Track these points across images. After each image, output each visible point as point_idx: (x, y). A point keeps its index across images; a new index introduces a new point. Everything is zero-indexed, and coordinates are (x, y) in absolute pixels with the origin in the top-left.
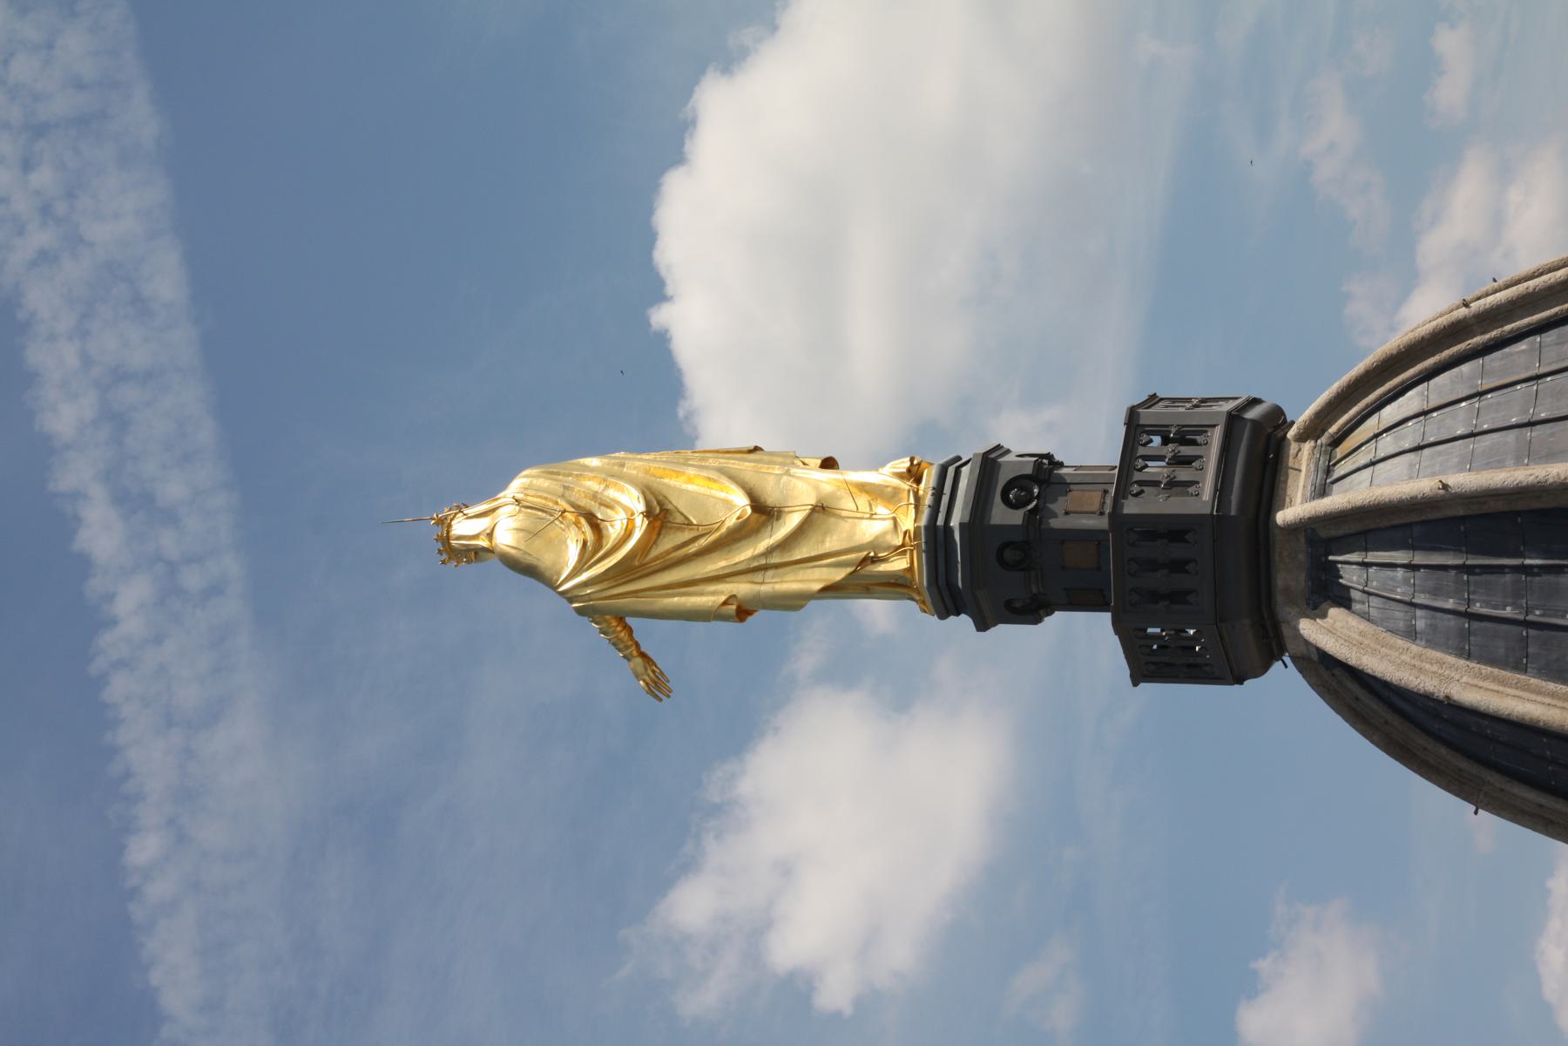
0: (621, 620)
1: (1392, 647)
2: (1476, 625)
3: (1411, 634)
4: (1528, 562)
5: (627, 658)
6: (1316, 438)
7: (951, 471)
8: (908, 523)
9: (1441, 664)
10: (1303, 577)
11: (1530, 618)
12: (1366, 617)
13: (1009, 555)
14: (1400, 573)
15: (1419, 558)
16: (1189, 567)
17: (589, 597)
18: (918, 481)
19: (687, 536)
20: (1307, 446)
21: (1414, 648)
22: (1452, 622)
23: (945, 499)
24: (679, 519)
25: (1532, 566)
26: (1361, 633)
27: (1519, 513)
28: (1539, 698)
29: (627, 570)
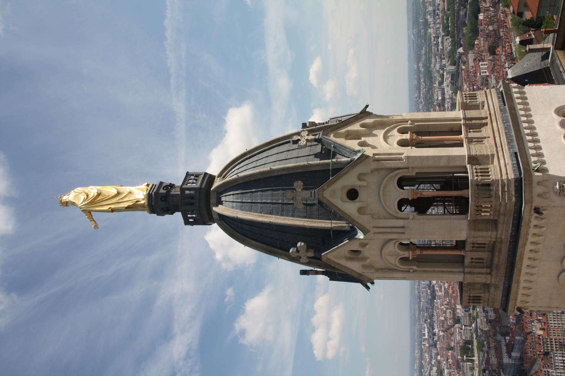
0: (90, 213)
1: (229, 210)
2: (243, 204)
3: (233, 207)
4: (252, 190)
5: (91, 221)
6: (220, 177)
9: (237, 212)
10: (215, 200)
11: (253, 201)
12: (226, 206)
13: (163, 199)
14: (231, 196)
15: (235, 192)
16: (194, 198)
17: (83, 208)
20: (219, 178)
21: (233, 210)
22: (239, 204)
23: (152, 189)
25: (253, 191)
26: (224, 209)
27: (251, 181)
28: (253, 216)
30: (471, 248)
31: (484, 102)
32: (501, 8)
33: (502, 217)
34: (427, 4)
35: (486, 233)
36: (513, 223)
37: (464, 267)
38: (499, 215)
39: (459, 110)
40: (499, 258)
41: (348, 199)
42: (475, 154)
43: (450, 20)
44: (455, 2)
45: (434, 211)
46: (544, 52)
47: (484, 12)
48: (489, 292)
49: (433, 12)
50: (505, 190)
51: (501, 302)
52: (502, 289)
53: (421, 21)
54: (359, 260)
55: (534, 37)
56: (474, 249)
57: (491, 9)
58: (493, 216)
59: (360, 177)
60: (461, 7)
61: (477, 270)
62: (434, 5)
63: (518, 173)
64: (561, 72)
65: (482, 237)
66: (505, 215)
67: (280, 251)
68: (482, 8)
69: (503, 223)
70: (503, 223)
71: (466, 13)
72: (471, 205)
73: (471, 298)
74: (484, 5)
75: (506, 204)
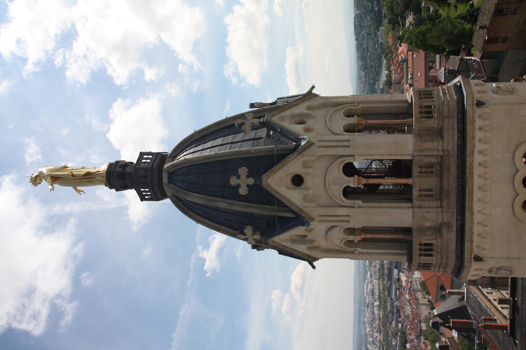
13: (120, 177)
30: (419, 174)
32: (423, 340)
33: (446, 121)
34: (368, 337)
36: (458, 127)
38: (443, 118)
41: (293, 185)
43: (385, 348)
44: (389, 335)
46: (460, 295)
47: (410, 342)
48: (441, 236)
49: (373, 342)
50: (446, 92)
51: (456, 251)
52: (455, 229)
53: (363, 348)
54: (304, 242)
55: (449, 344)
56: (422, 174)
57: (415, 340)
58: (438, 120)
59: (305, 165)
60: (393, 339)
62: (373, 337)
64: (476, 297)
65: (429, 150)
66: (448, 117)
67: (220, 199)
68: (408, 339)
69: (448, 128)
70: (448, 128)
71: (397, 343)
72: (415, 105)
73: (421, 265)
74: (410, 337)
75: (448, 102)
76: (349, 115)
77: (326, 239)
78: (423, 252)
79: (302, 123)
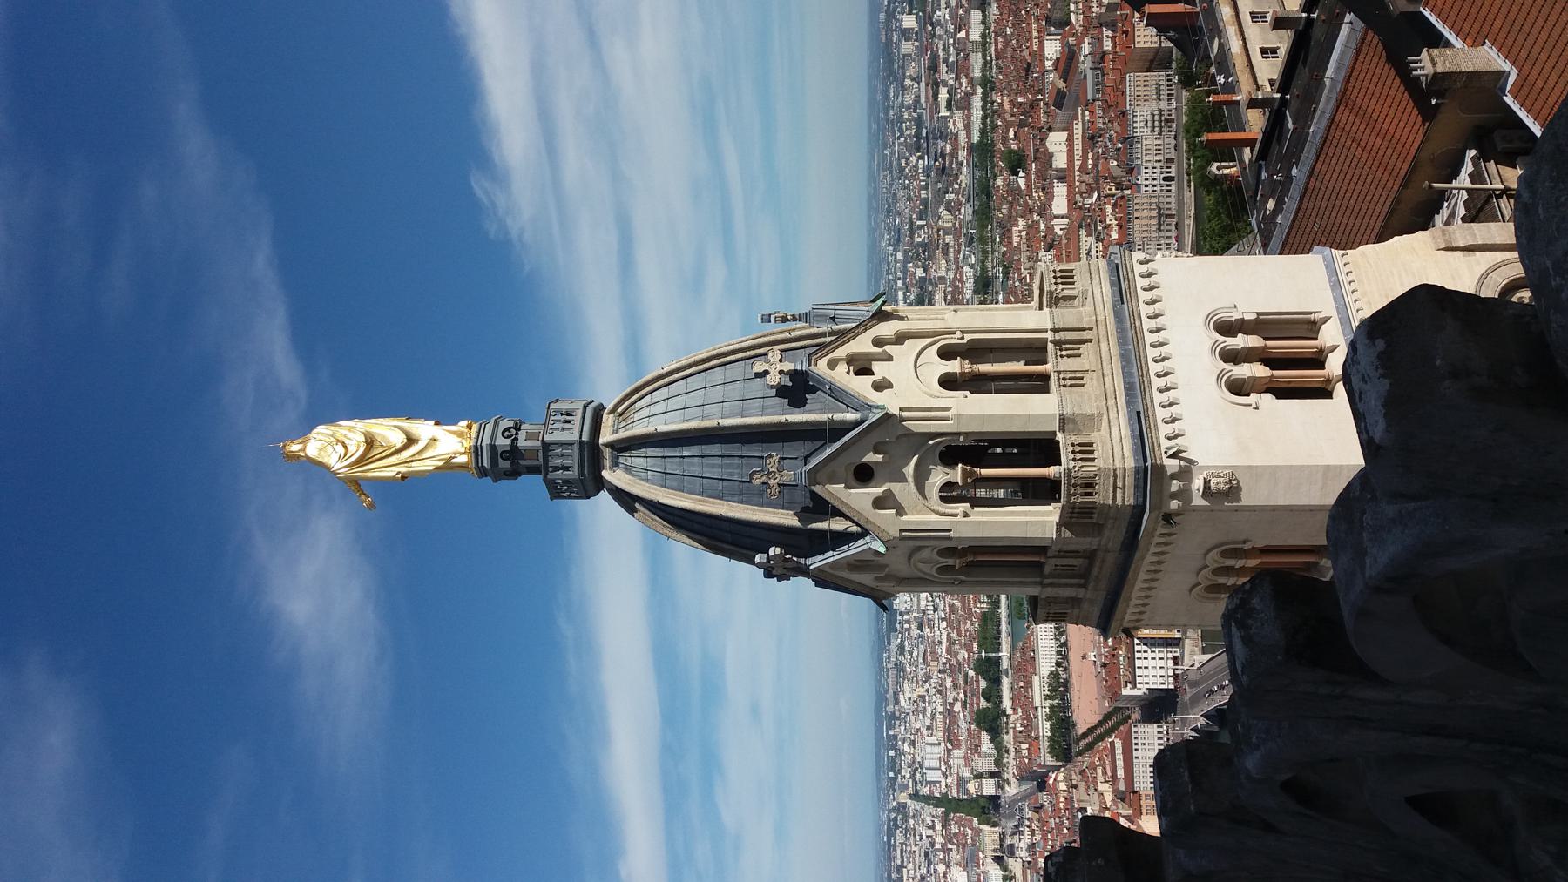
3: (647, 480)
7: (483, 425)
8: (467, 444)
9: (656, 490)
18: (470, 429)
19: (381, 450)
20: (612, 415)
21: (647, 485)
23: (748, 354)
24: (379, 444)
26: (630, 480)
29: (361, 461)
31: (1086, 290)
33: (1111, 521)
35: (1083, 539)
37: (1042, 576)
39: (1041, 308)
40: (1101, 568)
42: (1072, 412)
45: (921, 162)
61: (1063, 581)
63: (1141, 499)
76: (946, 354)
77: (909, 562)
78: (1079, 456)
79: (865, 371)
